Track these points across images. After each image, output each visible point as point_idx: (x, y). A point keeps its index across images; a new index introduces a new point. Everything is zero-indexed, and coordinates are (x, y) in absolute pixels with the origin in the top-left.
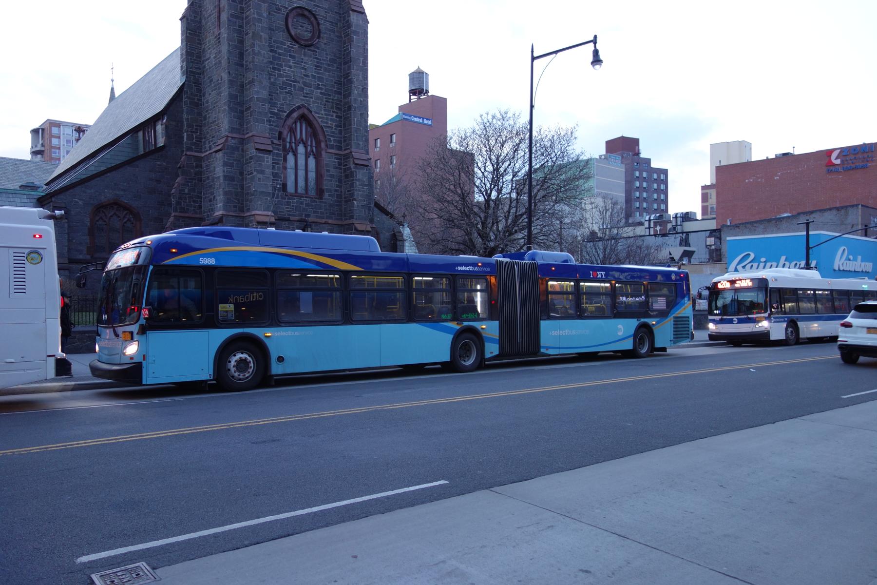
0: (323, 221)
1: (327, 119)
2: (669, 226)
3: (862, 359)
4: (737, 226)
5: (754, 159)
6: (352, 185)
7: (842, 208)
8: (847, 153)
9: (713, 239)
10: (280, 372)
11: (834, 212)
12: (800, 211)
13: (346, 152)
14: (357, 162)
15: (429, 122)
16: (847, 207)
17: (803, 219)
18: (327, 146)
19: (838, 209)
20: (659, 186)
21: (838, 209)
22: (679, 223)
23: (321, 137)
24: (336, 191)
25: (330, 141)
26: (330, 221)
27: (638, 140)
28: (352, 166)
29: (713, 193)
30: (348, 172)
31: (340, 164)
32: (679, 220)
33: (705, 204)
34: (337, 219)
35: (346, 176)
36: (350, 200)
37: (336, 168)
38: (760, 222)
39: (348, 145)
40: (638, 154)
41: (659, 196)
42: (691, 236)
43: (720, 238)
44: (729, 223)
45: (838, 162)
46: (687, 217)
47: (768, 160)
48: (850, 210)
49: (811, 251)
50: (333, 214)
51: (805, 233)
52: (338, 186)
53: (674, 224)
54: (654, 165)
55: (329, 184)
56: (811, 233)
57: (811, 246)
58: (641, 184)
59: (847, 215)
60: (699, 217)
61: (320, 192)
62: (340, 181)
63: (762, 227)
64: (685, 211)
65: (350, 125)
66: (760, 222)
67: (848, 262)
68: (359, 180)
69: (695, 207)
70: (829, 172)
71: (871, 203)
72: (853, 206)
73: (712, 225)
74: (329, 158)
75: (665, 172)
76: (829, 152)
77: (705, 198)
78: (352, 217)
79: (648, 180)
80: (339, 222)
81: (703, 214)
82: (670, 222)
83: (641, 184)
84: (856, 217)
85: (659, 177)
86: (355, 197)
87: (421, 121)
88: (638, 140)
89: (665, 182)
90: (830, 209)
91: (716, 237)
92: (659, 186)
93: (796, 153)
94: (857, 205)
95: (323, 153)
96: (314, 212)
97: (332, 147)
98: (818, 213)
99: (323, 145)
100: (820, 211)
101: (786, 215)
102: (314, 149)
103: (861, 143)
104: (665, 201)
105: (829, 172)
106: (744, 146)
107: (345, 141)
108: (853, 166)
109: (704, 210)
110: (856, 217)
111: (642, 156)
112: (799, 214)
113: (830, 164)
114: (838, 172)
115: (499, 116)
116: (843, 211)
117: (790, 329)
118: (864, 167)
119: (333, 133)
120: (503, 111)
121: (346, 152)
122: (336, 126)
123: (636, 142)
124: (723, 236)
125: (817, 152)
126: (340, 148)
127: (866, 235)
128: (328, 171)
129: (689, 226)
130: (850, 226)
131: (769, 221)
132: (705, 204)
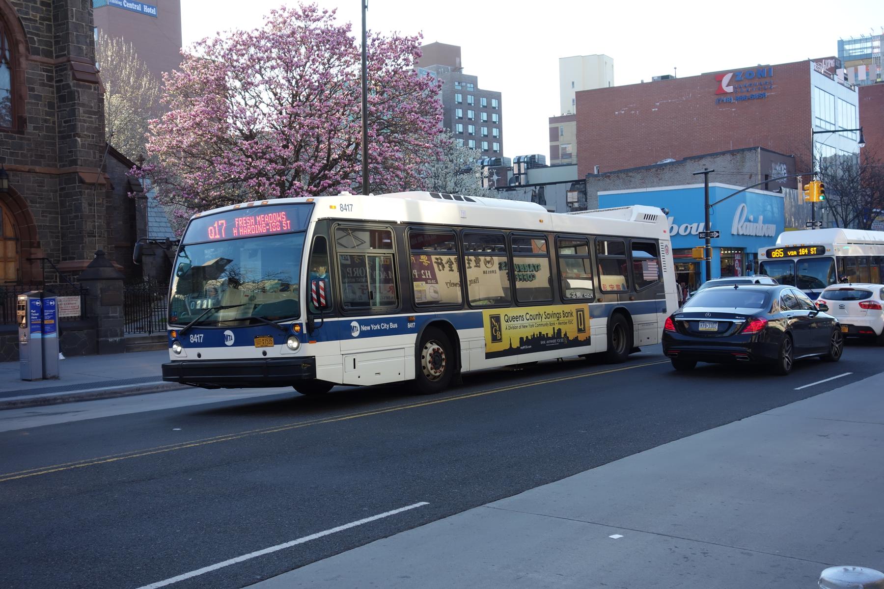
0: (27, 168)
1: (27, 7)
2: (510, 175)
3: (700, 364)
4: (606, 176)
5: (618, 82)
6: (73, 113)
7: (738, 151)
8: (742, 77)
9: (576, 194)
10: (604, 337)
11: (728, 157)
12: (686, 155)
13: (61, 60)
14: (79, 76)
15: (153, 11)
16: (743, 150)
17: (699, 166)
18: (27, 49)
19: (733, 153)
20: (489, 116)
21: (733, 153)
22: (523, 171)
23: (19, 37)
24: (46, 121)
25: (34, 42)
26: (37, 169)
27: (562, 60)
28: (72, 83)
29: (570, 130)
30: (65, 92)
31: (50, 79)
32: (523, 166)
33: (555, 143)
34: (49, 166)
35: (62, 99)
36: (69, 136)
37: (43, 85)
38: (637, 170)
39: (63, 49)
40: (460, 69)
41: (490, 131)
42: (547, 189)
43: (585, 193)
44: (596, 172)
45: (730, 89)
46: (533, 162)
47: (643, 86)
48: (748, 155)
49: (711, 209)
50: (42, 157)
51: (703, 185)
52: (47, 114)
53: (516, 171)
54: (481, 86)
55: (36, 109)
56: (710, 185)
57: (710, 203)
58: (465, 113)
59: (743, 161)
60: (548, 163)
61: (19, 123)
62: (51, 105)
63: (639, 176)
64: (530, 153)
65: (66, 17)
66: (637, 170)
67: (748, 224)
68: (83, 105)
69: (542, 148)
70: (719, 102)
71: (770, 145)
72: (750, 149)
73: (572, 173)
74: (33, 68)
75: (498, 96)
76: (718, 77)
77: (554, 135)
78: (74, 162)
79: (478, 110)
80: (53, 170)
81: (552, 158)
82: (511, 169)
83: (465, 113)
84: (754, 163)
85: (489, 103)
86: (79, 131)
87: (139, 8)
88: (562, 60)
89: (499, 111)
90: (723, 154)
91: (580, 192)
92: (489, 116)
93: (678, 77)
94: (755, 149)
95: (23, 60)
96: (12, 154)
97: (36, 52)
98: (709, 159)
99: (22, 48)
100: (712, 155)
101: (669, 161)
102: (7, 53)
103: (755, 65)
104: (499, 140)
105: (719, 102)
106: (602, 62)
107: (57, 43)
108: (748, 95)
109: (554, 151)
110: (754, 163)
111: (464, 72)
112: (685, 159)
113: (721, 92)
114: (729, 102)
115: (301, 13)
116: (739, 156)
117: (431, 347)
118: (761, 97)
119: (37, 29)
120: (306, 5)
121: (61, 60)
122: (42, 18)
123: (455, 52)
124: (590, 190)
125: (703, 75)
126: (48, 54)
127: (767, 189)
128: (32, 90)
129: (538, 176)
130: (747, 177)
131: (648, 168)
132: (555, 143)
